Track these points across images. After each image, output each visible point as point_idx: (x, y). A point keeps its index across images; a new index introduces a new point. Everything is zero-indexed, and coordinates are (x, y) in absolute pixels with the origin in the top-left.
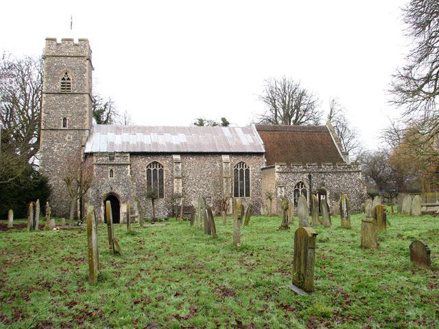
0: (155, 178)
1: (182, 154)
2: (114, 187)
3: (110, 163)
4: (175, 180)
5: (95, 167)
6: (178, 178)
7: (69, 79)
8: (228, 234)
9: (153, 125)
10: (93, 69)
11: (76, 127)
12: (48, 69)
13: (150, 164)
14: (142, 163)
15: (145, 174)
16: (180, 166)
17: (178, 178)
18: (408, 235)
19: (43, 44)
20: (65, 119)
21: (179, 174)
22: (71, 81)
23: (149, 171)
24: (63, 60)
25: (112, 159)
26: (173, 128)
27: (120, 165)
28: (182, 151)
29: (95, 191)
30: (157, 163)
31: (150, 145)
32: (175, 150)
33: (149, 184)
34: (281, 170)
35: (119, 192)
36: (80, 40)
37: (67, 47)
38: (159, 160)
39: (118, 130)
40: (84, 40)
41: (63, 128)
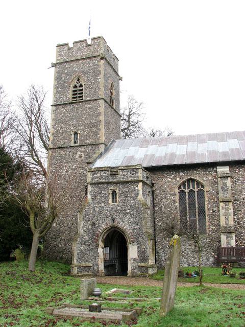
0: (192, 205)
2: (118, 217)
3: (111, 180)
4: (221, 204)
5: (90, 188)
6: (226, 202)
7: (81, 86)
8: (35, 291)
9: (194, 133)
10: (121, 79)
11: (88, 142)
13: (183, 184)
14: (170, 184)
15: (177, 198)
16: (228, 182)
17: (226, 202)
18: (15, 310)
19: (54, 51)
20: (76, 134)
21: (228, 196)
23: (182, 193)
24: (74, 64)
26: (222, 134)
27: (127, 182)
28: (231, 159)
29: (89, 225)
30: (193, 180)
31: (184, 155)
32: (219, 159)
33: (183, 210)
35: (125, 225)
36: (93, 39)
37: (80, 50)
38: (196, 175)
39: (145, 143)
40: (98, 38)
41: (73, 145)
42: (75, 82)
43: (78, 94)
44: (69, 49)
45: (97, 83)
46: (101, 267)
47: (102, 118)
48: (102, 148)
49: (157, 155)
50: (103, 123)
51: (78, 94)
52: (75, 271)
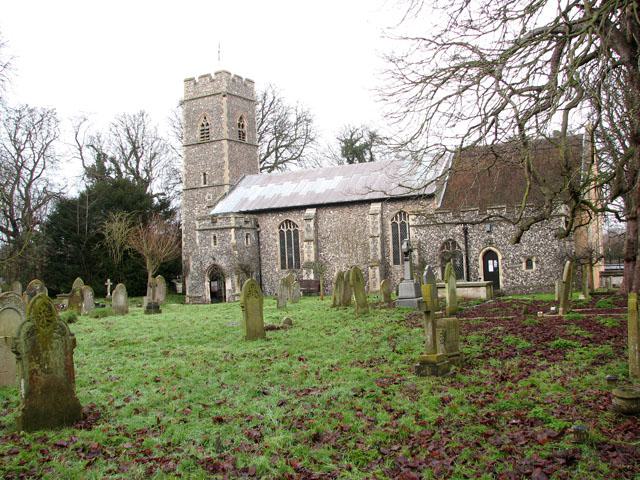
1: (318, 206)
7: (207, 124)
11: (215, 182)
12: (187, 117)
13: (282, 224)
14: (271, 224)
15: (278, 237)
20: (205, 174)
22: (245, 128)
23: (281, 232)
25: (214, 222)
28: (317, 202)
29: (198, 264)
32: (308, 203)
34: (417, 222)
35: (222, 263)
36: (216, 74)
38: (292, 217)
42: (202, 121)
43: (205, 133)
44: (195, 84)
45: (220, 122)
46: (209, 297)
47: (226, 159)
48: (227, 189)
49: (318, 191)
50: (227, 164)
51: (205, 133)
52: (188, 300)
